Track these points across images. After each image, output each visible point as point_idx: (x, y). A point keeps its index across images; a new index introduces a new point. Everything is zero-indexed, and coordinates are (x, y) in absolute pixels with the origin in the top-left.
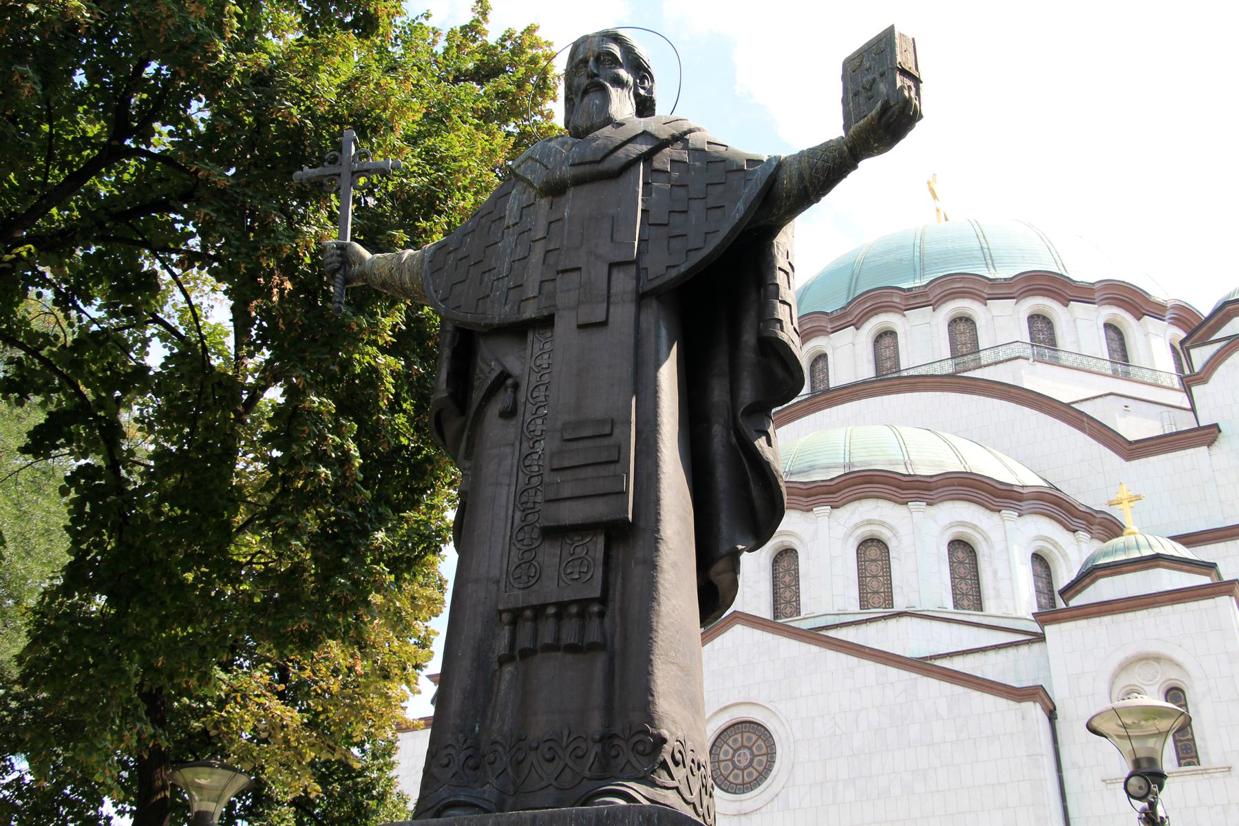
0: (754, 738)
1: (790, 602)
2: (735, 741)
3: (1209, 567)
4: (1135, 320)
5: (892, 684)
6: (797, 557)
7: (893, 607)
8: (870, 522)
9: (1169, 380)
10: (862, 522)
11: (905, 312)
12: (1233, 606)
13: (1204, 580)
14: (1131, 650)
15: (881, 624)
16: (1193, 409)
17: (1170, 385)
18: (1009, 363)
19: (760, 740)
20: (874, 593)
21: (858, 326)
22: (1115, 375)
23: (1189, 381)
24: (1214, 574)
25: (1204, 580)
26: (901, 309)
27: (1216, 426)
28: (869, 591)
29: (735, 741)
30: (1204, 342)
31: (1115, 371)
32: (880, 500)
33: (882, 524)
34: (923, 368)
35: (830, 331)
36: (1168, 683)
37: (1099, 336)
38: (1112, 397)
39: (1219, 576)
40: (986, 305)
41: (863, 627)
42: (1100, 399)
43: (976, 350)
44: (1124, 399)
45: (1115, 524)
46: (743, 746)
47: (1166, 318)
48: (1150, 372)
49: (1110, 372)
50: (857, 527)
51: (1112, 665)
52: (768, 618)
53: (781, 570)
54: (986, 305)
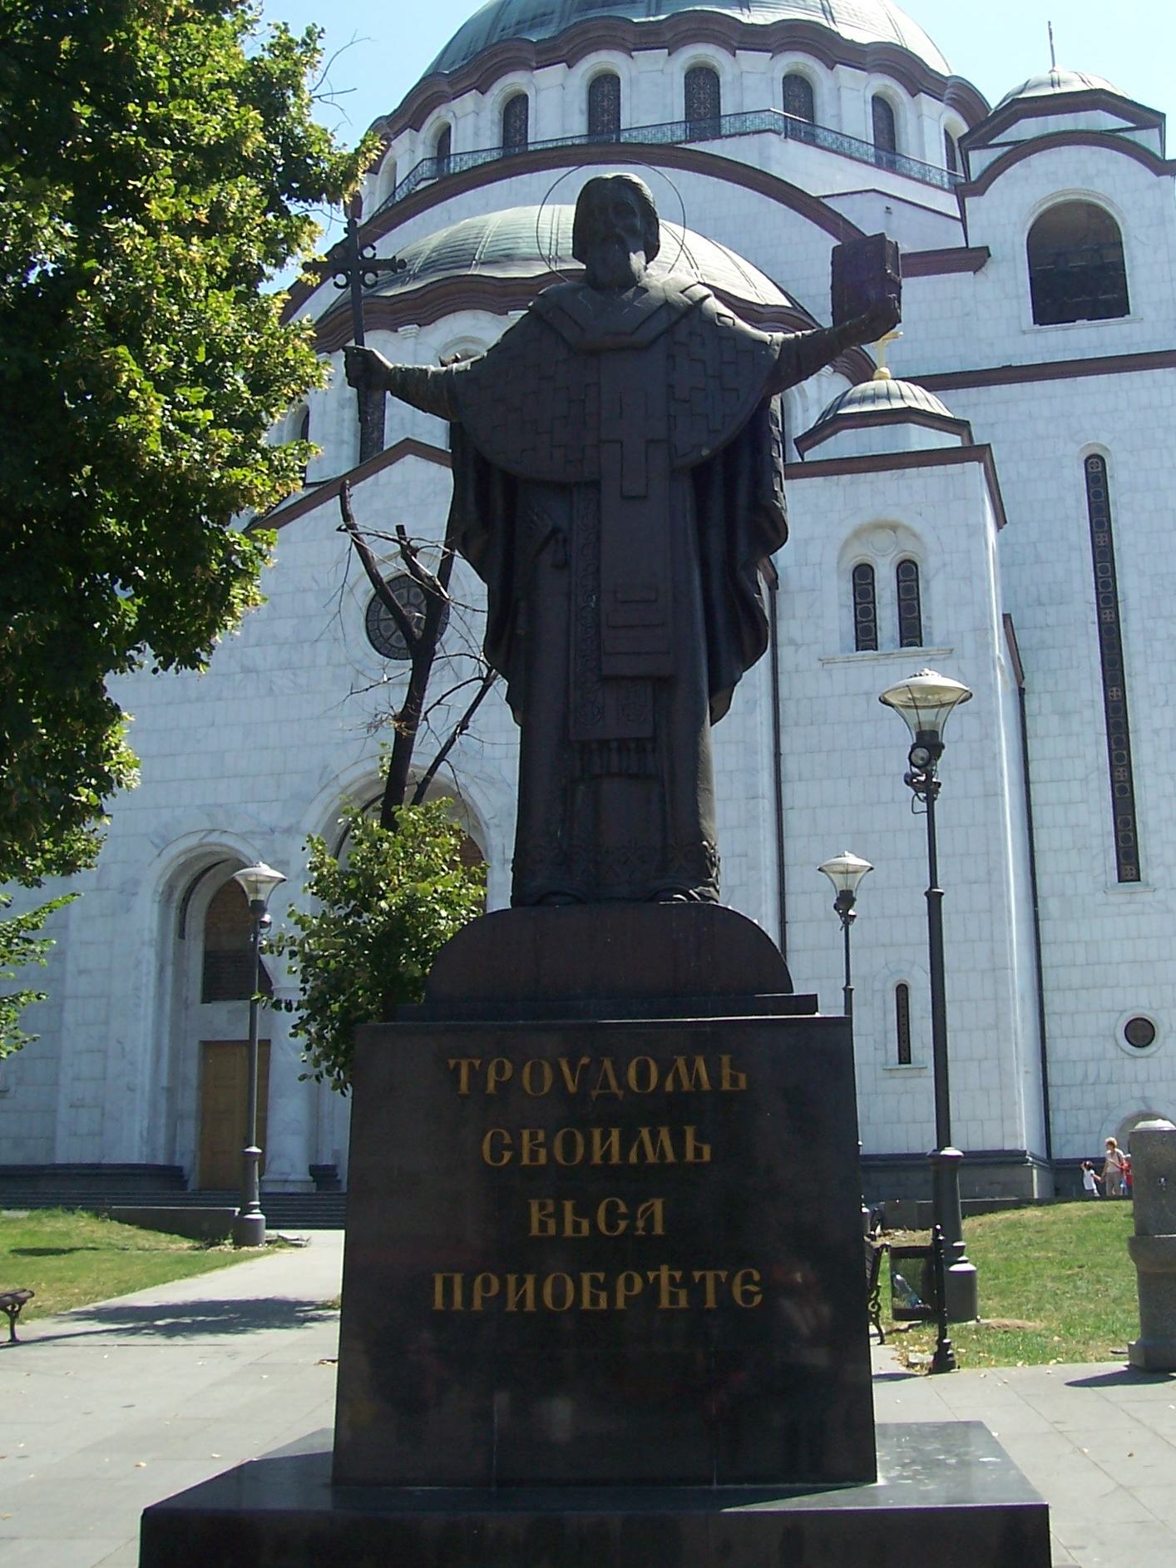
3: (958, 426)
4: (909, 96)
9: (938, 177)
11: (634, 53)
12: (981, 482)
13: (953, 441)
14: (866, 517)
16: (963, 220)
17: (939, 184)
18: (756, 136)
22: (878, 165)
23: (965, 190)
24: (965, 433)
25: (953, 441)
27: (987, 248)
30: (983, 145)
35: (534, 64)
36: (901, 555)
37: (865, 112)
38: (873, 194)
39: (971, 439)
40: (734, 55)
43: (717, 115)
45: (863, 357)
47: (945, 98)
48: (919, 165)
49: (873, 160)
51: (845, 532)
54: (734, 55)
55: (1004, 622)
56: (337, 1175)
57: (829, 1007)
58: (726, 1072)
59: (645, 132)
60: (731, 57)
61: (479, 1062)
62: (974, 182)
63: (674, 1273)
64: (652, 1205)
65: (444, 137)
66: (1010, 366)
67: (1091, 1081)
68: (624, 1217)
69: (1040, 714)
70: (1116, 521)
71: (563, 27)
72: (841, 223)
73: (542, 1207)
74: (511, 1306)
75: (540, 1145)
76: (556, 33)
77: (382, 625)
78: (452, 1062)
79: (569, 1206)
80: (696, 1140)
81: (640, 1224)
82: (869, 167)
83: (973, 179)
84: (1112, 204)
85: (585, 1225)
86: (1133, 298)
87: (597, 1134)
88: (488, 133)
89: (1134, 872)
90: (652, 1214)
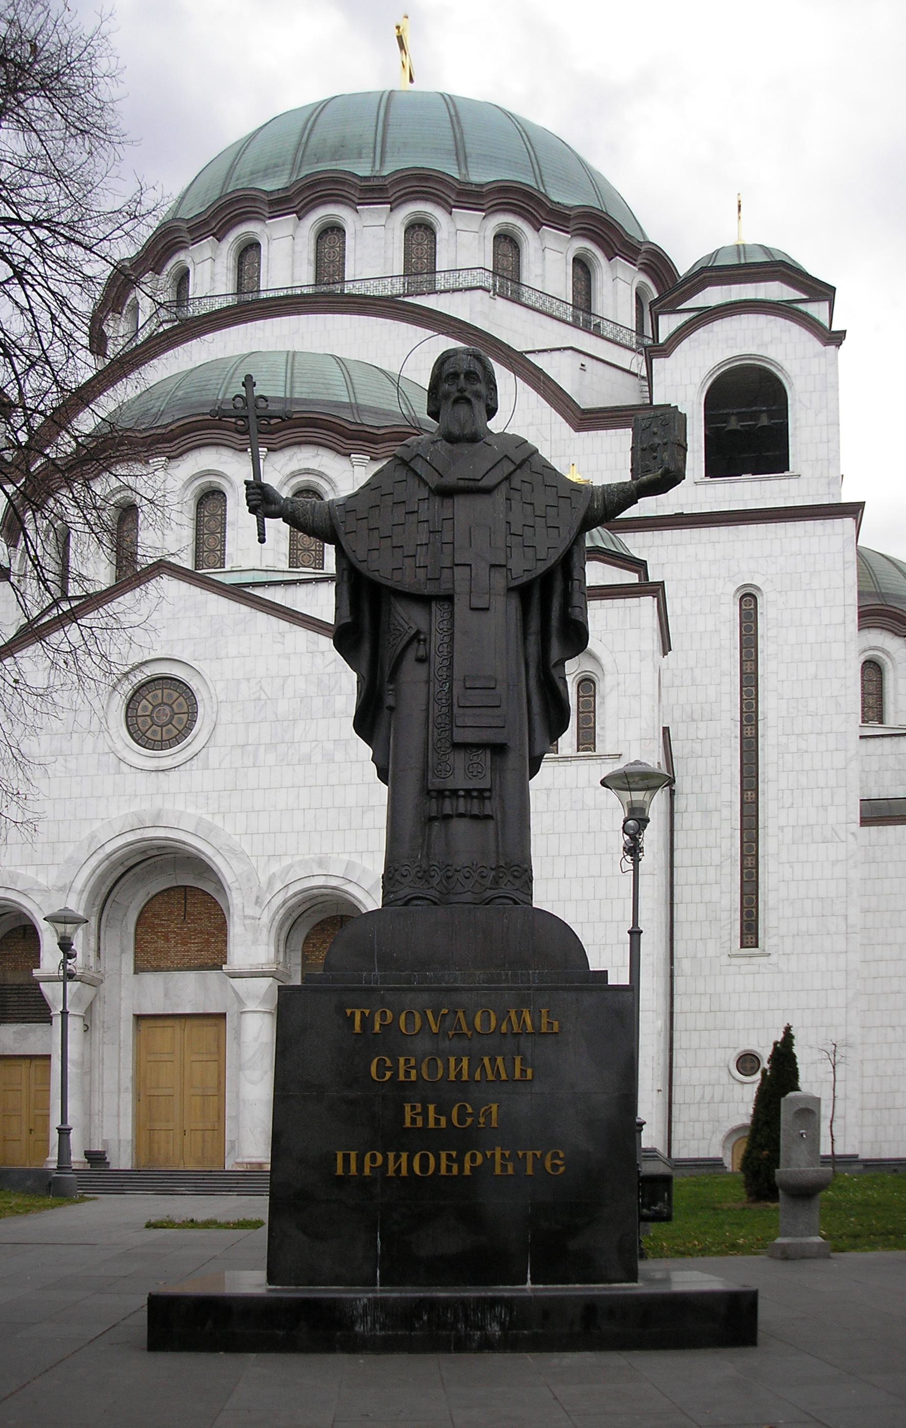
0: (176, 695)
1: (213, 551)
2: (155, 696)
5: (323, 653)
6: (225, 501)
7: (323, 569)
8: (308, 471)
10: (299, 470)
13: (632, 578)
15: (310, 587)
18: (468, 292)
19: (181, 698)
20: (305, 550)
21: (300, 215)
22: (574, 325)
25: (632, 578)
26: (353, 202)
28: (300, 547)
29: (155, 696)
31: (576, 318)
32: (320, 447)
33: (321, 475)
34: (372, 282)
35: (268, 215)
38: (570, 352)
39: (647, 578)
40: (450, 213)
41: (292, 588)
42: (558, 353)
44: (582, 356)
46: (163, 703)
48: (611, 326)
49: (570, 319)
50: (293, 475)
52: (191, 569)
53: (206, 514)
54: (450, 213)
55: (664, 734)
56: (106, 1158)
57: (619, 977)
58: (544, 1020)
59: (368, 283)
60: (447, 215)
61: (369, 1011)
62: (662, 345)
63: (504, 1152)
64: (491, 1107)
65: (183, 278)
66: (682, 513)
67: (707, 1099)
68: (470, 1115)
69: (686, 811)
70: (762, 652)
71: (294, 178)
72: (542, 377)
73: (413, 1108)
74: (391, 1173)
75: (411, 1067)
76: (288, 185)
77: (140, 720)
78: (349, 1011)
79: (431, 1108)
80: (436, 1113)
81: (482, 1120)
82: (567, 326)
83: (661, 341)
84: (782, 369)
85: (443, 1120)
86: (793, 456)
87: (452, 1061)
88: (224, 279)
89: (754, 940)
90: (491, 1112)
